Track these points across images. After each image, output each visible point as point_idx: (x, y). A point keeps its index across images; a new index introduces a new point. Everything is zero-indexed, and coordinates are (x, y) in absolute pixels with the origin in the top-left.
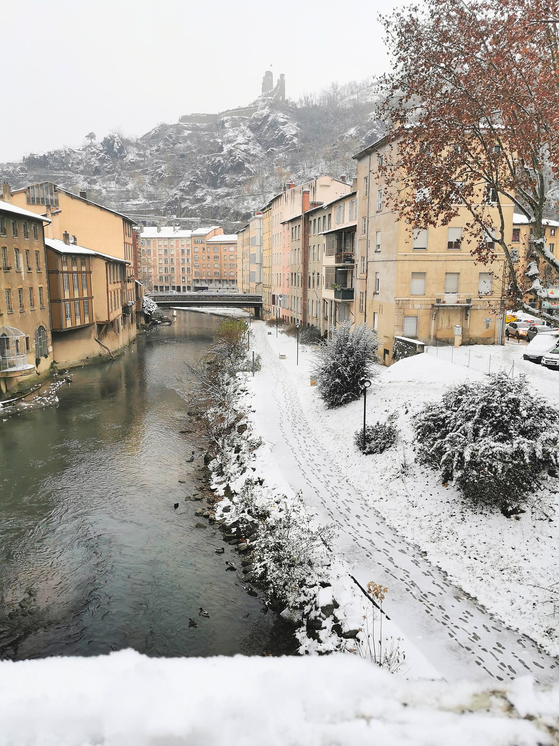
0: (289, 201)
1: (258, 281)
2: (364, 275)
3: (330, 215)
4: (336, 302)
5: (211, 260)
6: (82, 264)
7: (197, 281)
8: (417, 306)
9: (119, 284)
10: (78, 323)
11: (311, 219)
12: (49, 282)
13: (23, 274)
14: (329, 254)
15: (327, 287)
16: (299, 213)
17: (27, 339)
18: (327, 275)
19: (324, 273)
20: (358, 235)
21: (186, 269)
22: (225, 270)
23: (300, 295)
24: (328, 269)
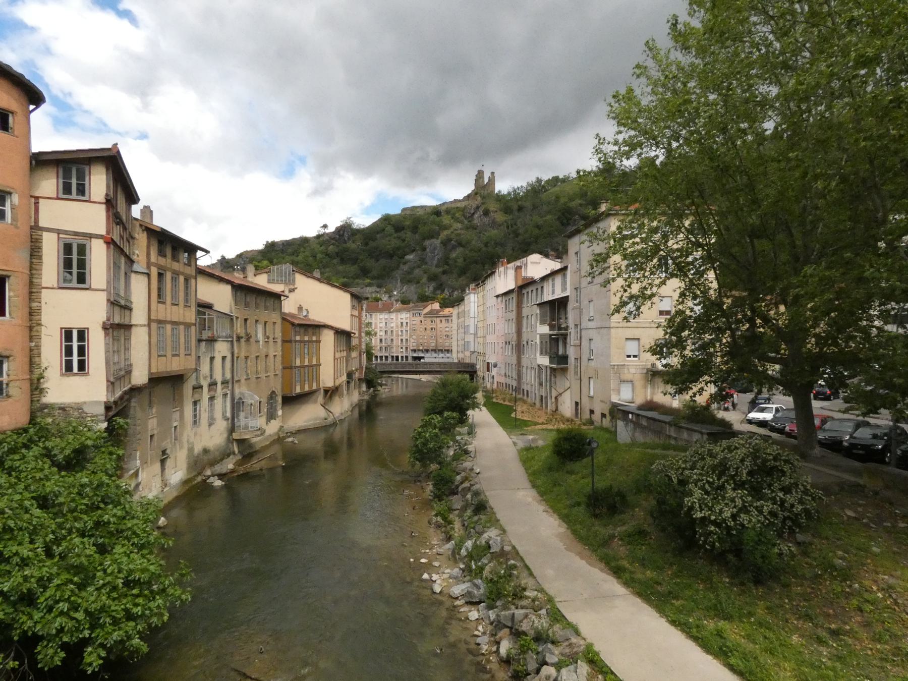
0: (502, 276)
1: (472, 350)
2: (578, 342)
3: (542, 287)
4: (551, 368)
5: (428, 331)
6: (313, 334)
7: (414, 351)
8: (633, 370)
9: (345, 352)
10: (307, 389)
11: (525, 291)
12: (283, 350)
13: (261, 343)
14: (543, 322)
15: (541, 353)
16: (511, 285)
17: (260, 402)
18: (541, 342)
19: (538, 341)
20: (571, 305)
21: (404, 340)
22: (441, 341)
23: (514, 361)
24: (542, 336)
